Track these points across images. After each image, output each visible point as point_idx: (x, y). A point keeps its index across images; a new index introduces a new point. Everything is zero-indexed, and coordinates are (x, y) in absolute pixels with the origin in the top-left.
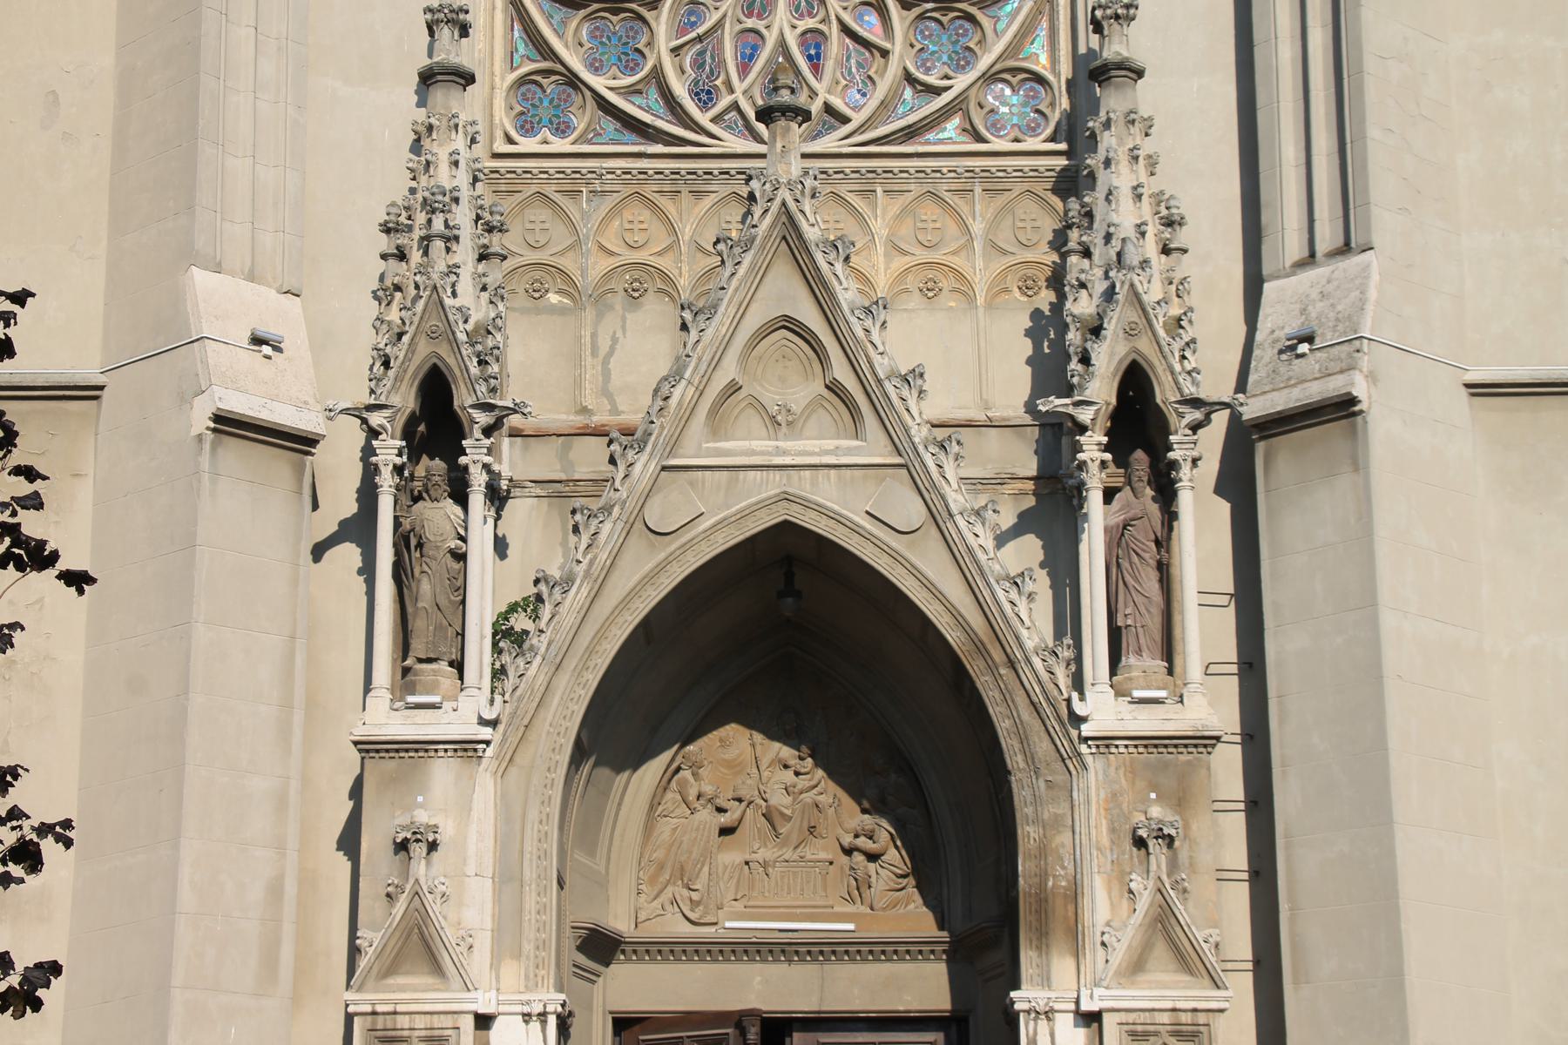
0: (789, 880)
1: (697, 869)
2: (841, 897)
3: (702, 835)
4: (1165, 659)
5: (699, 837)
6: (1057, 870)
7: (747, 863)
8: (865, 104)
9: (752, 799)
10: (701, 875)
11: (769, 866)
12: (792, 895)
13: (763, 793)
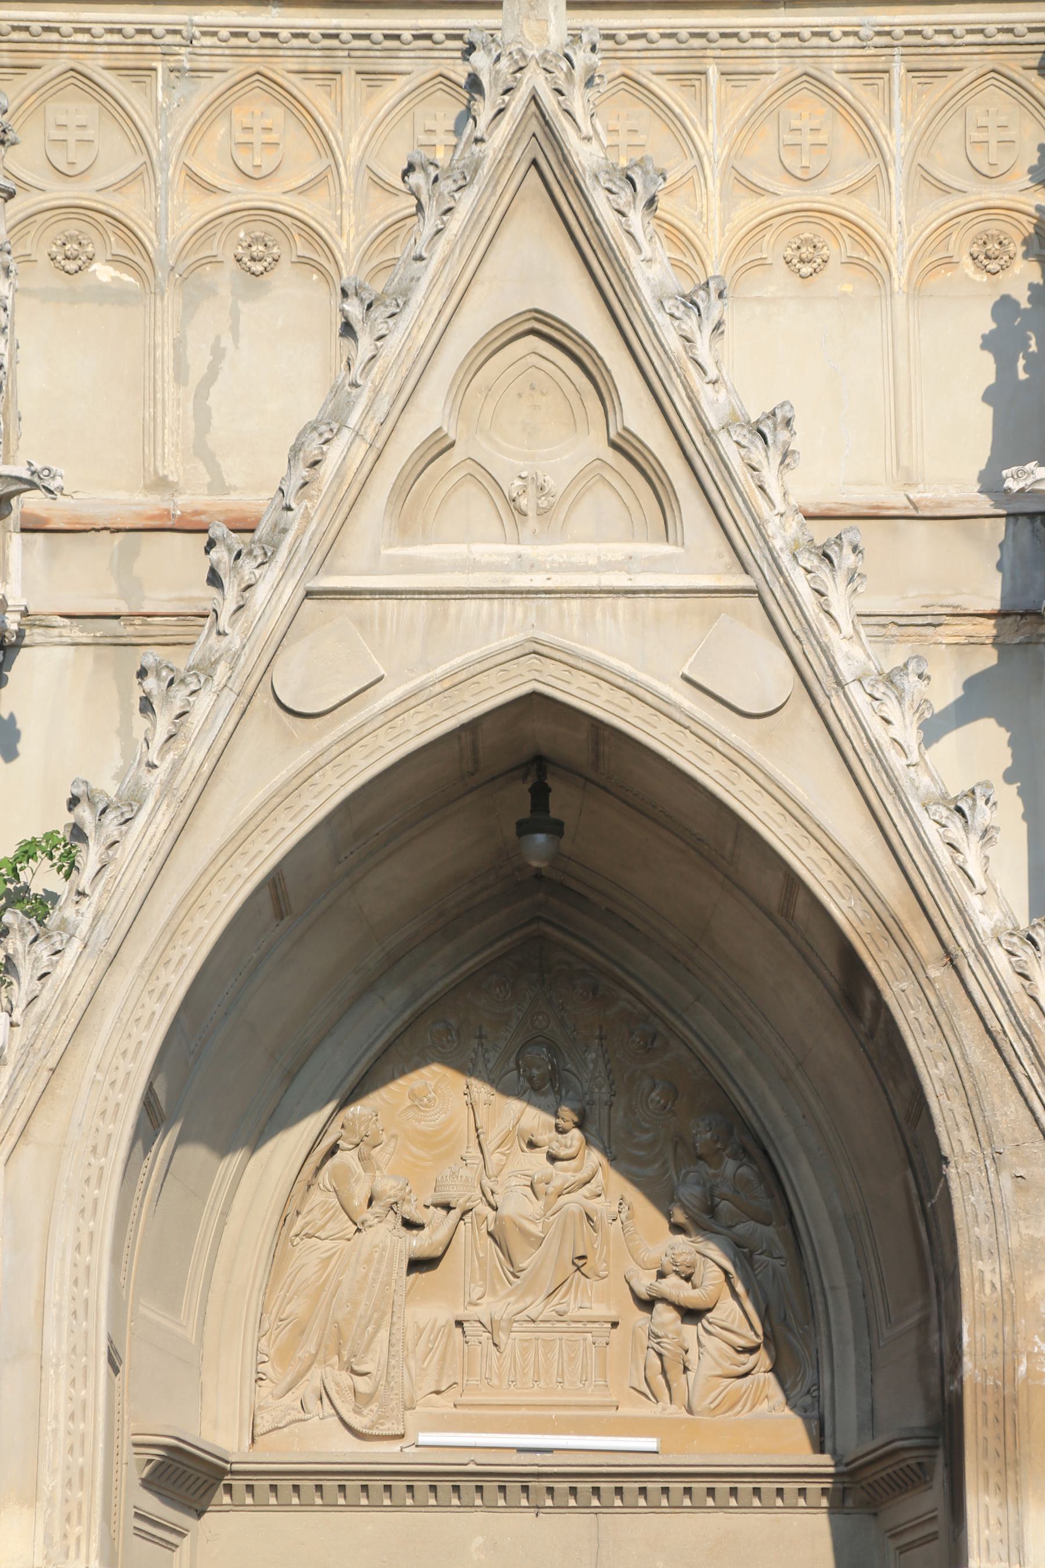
0: (537, 1354)
3: (377, 1271)
5: (371, 1274)
6: (1036, 1343)
7: (459, 1323)
9: (469, 1205)
11: (500, 1328)
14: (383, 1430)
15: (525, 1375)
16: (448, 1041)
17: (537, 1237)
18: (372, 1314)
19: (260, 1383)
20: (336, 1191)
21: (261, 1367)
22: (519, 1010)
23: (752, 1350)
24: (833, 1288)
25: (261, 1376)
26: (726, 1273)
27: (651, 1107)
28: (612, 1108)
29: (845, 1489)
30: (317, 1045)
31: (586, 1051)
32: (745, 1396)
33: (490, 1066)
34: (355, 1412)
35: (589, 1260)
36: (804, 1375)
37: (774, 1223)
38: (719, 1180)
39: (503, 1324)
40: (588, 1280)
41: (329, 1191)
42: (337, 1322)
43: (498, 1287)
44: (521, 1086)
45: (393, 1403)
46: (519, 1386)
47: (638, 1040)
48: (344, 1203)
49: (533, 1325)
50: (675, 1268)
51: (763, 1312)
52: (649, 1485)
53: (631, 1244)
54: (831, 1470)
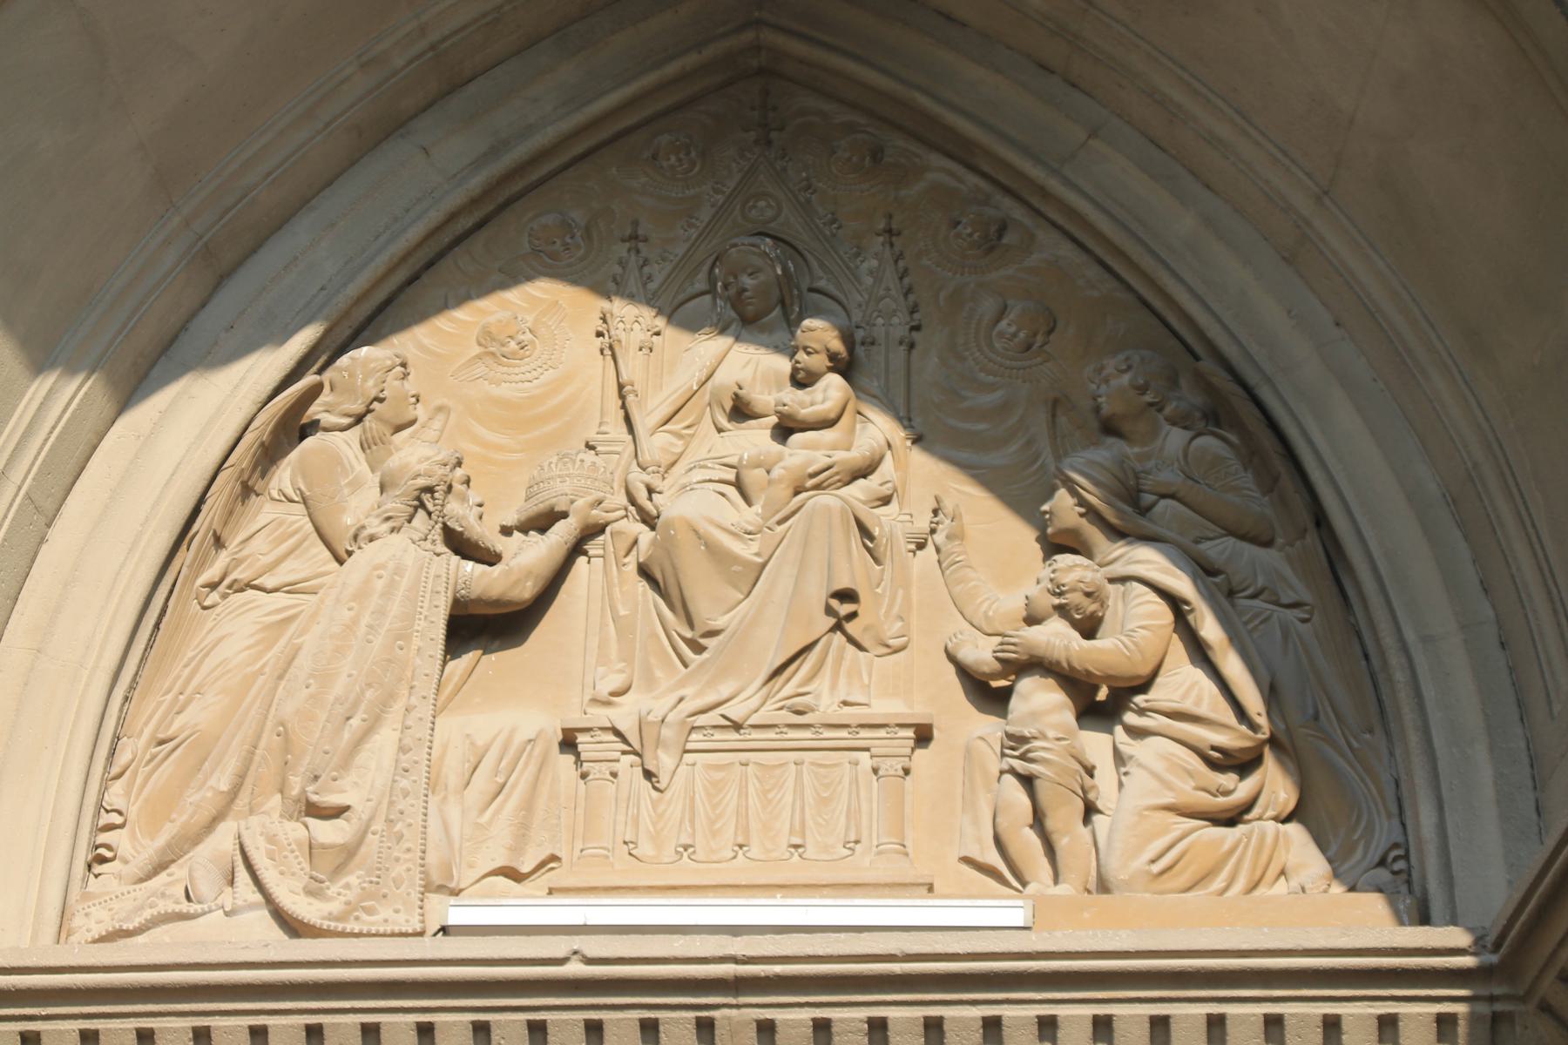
0: (743, 793)
1: (346, 735)
2: (967, 860)
3: (381, 613)
4: (1406, 918)
5: (366, 619)
7: (568, 743)
8: (710, 468)
9: (598, 515)
10: (362, 757)
12: (755, 851)
13: (642, 496)
14: (373, 924)
15: (714, 834)
16: (567, 247)
17: (746, 563)
18: (363, 692)
19: (97, 869)
20: (305, 501)
21: (103, 838)
22: (717, 191)
23: (1242, 763)
24: (1426, 640)
25: (102, 851)
26: (1175, 602)
27: (997, 345)
28: (914, 352)
29: (1496, 1018)
30: (279, 223)
31: (858, 255)
32: (1233, 860)
33: (652, 286)
34: (309, 892)
35: (863, 608)
36: (1370, 829)
37: (1280, 541)
38: (1150, 464)
39: (666, 732)
40: (861, 654)
41: (292, 501)
42: (282, 725)
43: (659, 673)
44: (720, 314)
45: (399, 870)
46: (700, 856)
47: (969, 230)
48: (322, 521)
49: (734, 735)
50: (1057, 601)
51: (1267, 691)
52: (1006, 1012)
53: (957, 589)
54: (1467, 961)
